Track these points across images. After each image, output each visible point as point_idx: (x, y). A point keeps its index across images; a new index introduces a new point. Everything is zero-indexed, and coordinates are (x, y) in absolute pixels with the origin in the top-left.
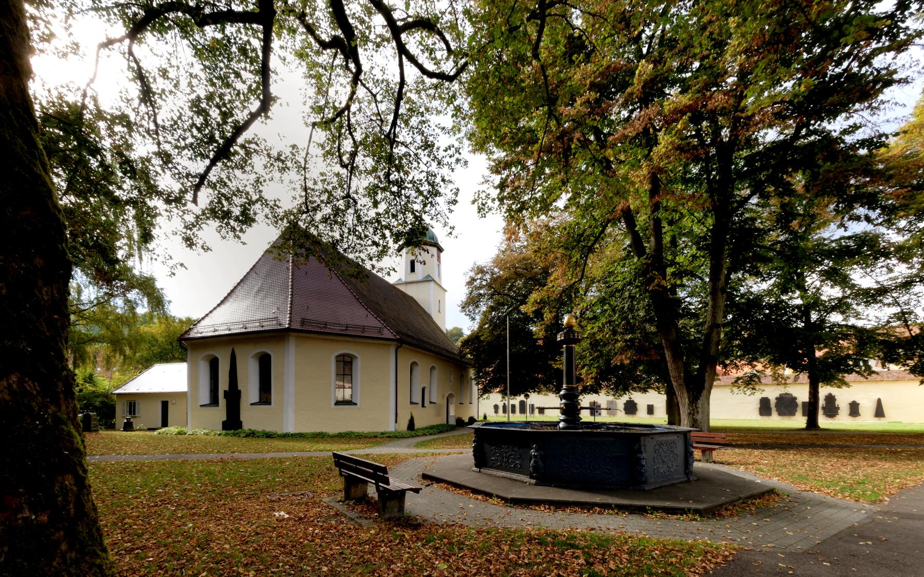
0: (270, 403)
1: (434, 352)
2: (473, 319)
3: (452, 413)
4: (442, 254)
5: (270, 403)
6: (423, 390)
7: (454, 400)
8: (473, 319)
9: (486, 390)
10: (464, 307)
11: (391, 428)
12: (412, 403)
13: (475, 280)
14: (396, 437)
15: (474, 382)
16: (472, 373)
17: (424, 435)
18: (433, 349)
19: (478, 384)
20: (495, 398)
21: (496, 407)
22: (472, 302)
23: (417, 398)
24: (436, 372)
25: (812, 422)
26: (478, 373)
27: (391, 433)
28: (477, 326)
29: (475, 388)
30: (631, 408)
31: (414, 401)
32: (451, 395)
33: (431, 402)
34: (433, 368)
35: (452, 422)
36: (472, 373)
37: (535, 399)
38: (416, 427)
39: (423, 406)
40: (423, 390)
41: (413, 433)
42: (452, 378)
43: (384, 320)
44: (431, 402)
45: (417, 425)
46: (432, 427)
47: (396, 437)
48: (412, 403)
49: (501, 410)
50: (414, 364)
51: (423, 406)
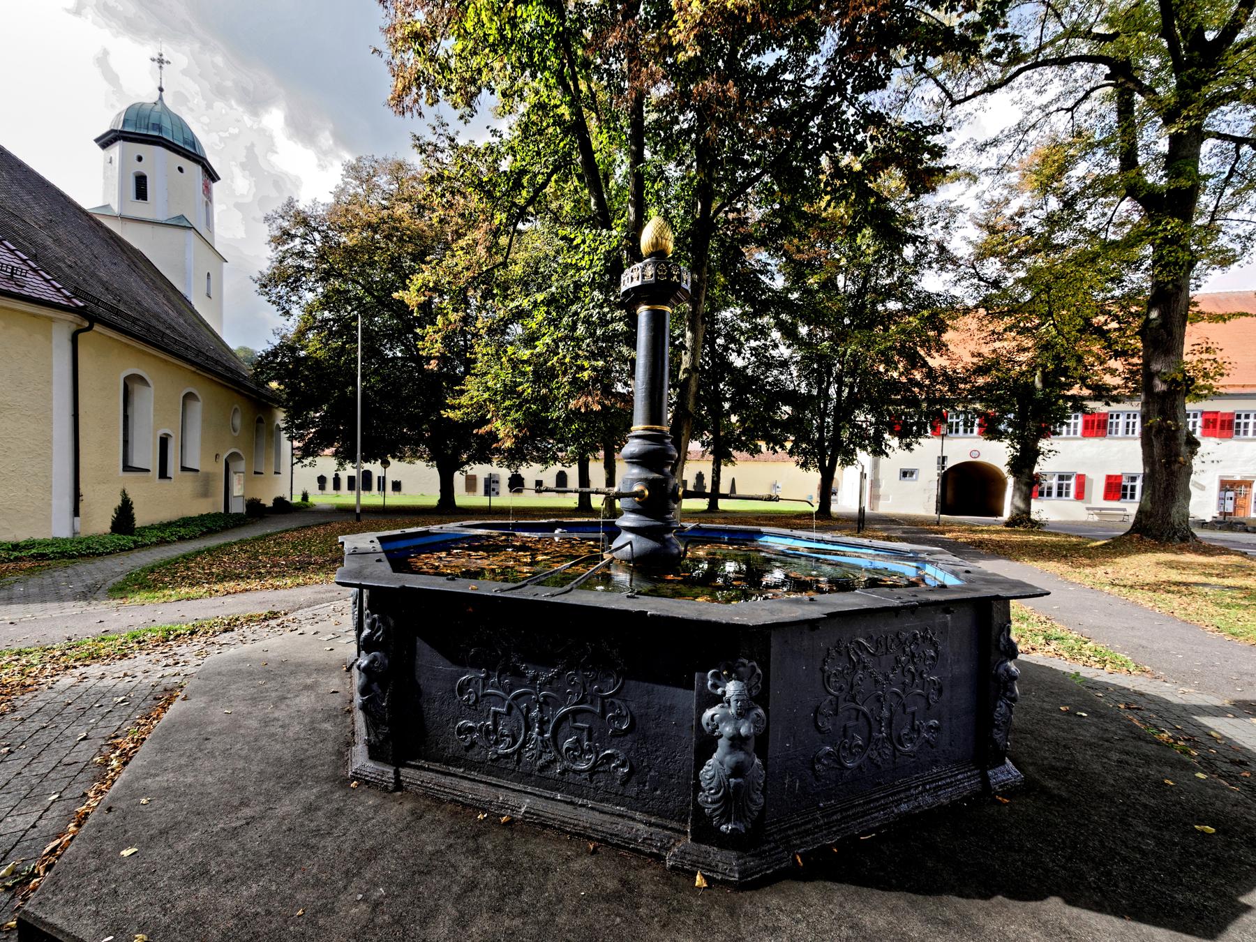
0: (1109, 477)
1: (192, 363)
2: (287, 313)
3: (237, 490)
4: (215, 186)
5: (1109, 477)
6: (164, 442)
7: (242, 466)
8: (287, 313)
9: (309, 451)
10: (266, 284)
11: (60, 527)
12: (127, 468)
13: (293, 237)
14: (63, 555)
15: (284, 436)
16: (280, 417)
17: (162, 542)
18: (191, 356)
19: (291, 439)
20: (326, 463)
21: (322, 480)
22: (283, 280)
23: (146, 455)
24: (197, 409)
25: (713, 506)
26: (291, 418)
27: (55, 542)
28: (293, 330)
29: (286, 446)
30: (516, 483)
31: (136, 462)
32: (234, 456)
33: (184, 469)
34: (189, 397)
35: (238, 507)
36: (280, 417)
37: (397, 469)
38: (138, 523)
39: (163, 474)
40: (164, 442)
41: (126, 540)
42: (238, 422)
43: (35, 258)
44: (184, 469)
45: (142, 517)
46: (186, 522)
47: (63, 555)
48: (127, 468)
49: (330, 484)
50: (131, 384)
51: (163, 474)
